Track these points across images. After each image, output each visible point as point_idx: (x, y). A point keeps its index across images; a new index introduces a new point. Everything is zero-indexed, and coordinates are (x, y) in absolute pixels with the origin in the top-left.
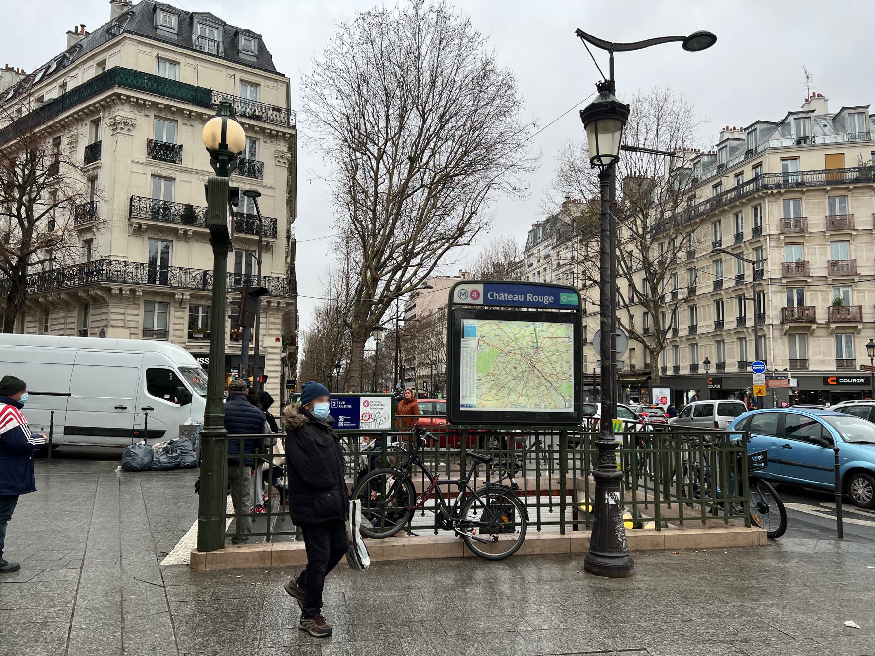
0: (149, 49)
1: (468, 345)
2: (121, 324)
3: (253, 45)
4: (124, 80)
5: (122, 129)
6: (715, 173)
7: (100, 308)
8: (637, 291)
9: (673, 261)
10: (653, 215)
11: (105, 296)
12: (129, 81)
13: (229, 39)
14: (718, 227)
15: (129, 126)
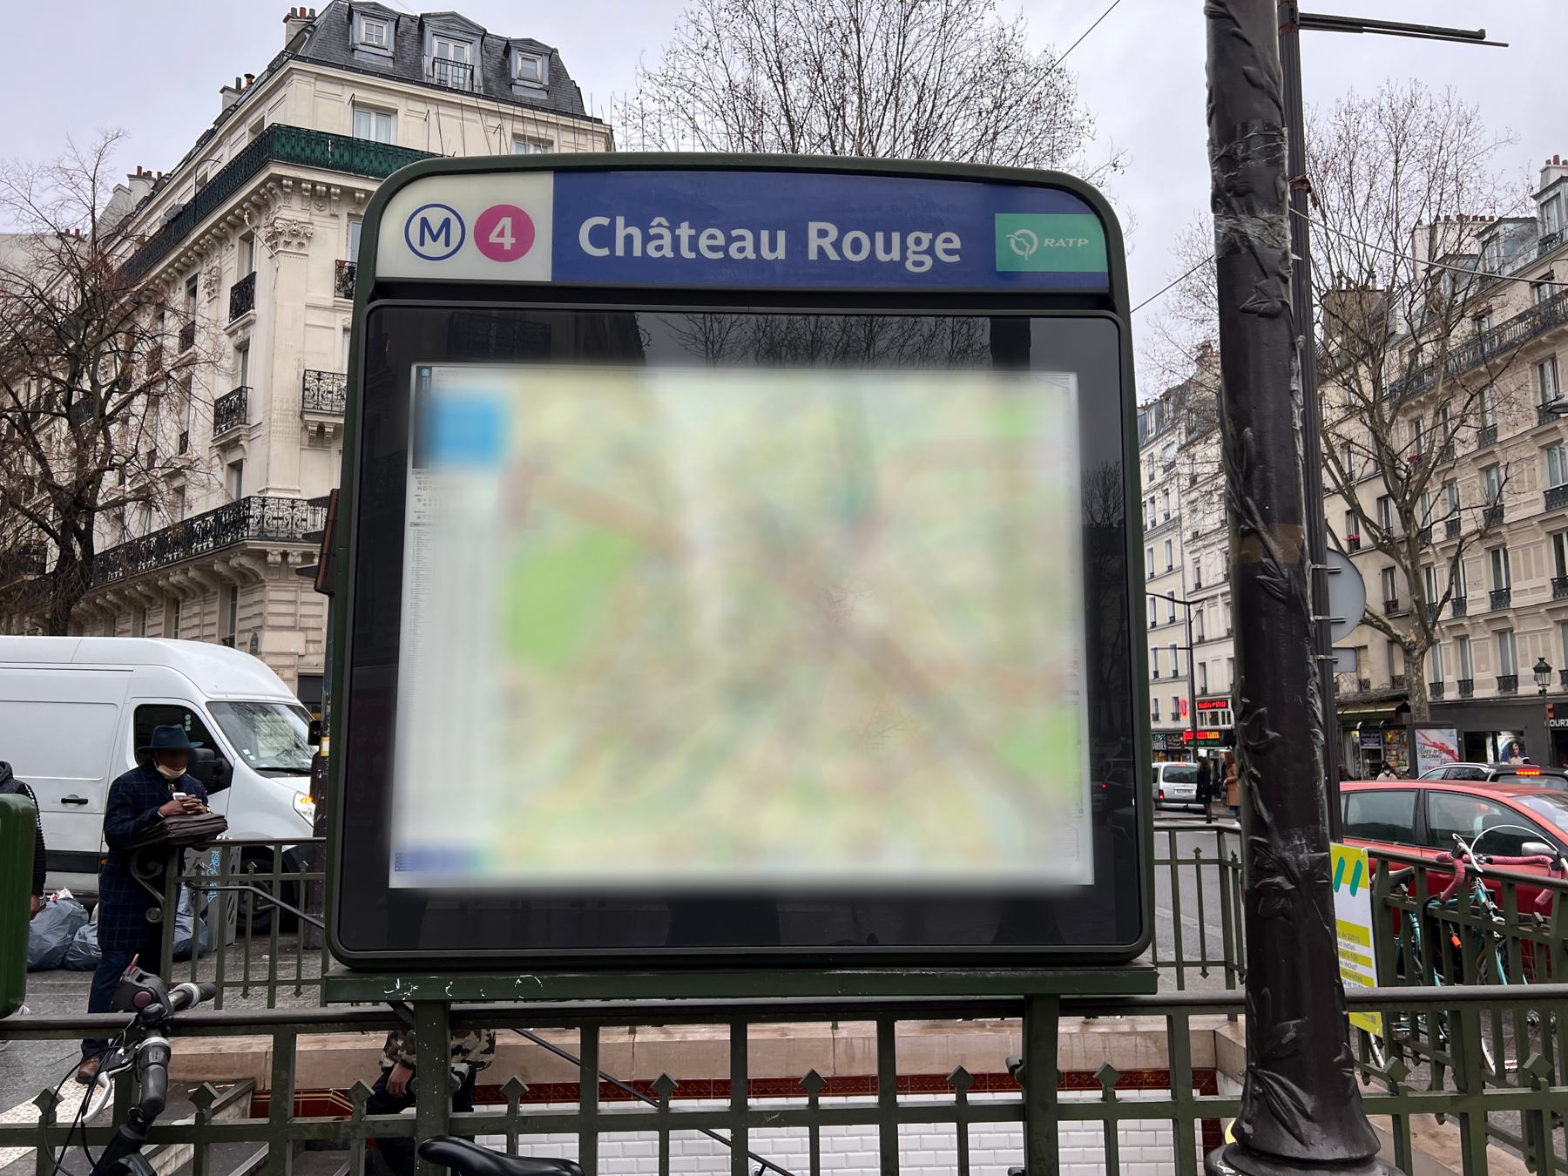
0: (337, 89)
1: (450, 509)
2: (288, 621)
3: (540, 68)
4: (288, 148)
5: (287, 243)
6: (1534, 255)
7: (252, 592)
8: (1366, 520)
9: (1448, 449)
10: (1393, 365)
11: (256, 568)
12: (298, 150)
13: (495, 63)
14: (1550, 379)
15: (300, 237)
